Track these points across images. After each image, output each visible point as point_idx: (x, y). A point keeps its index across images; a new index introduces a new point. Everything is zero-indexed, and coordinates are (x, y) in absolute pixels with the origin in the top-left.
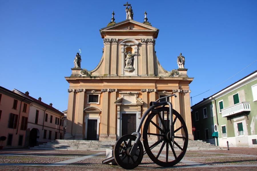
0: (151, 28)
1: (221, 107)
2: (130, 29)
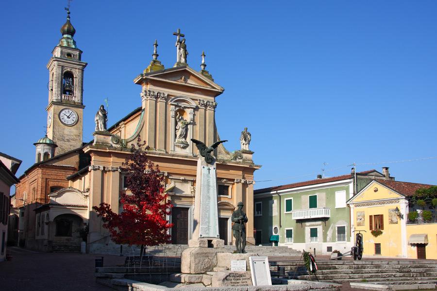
0: (215, 87)
1: (289, 208)
2: (185, 80)
